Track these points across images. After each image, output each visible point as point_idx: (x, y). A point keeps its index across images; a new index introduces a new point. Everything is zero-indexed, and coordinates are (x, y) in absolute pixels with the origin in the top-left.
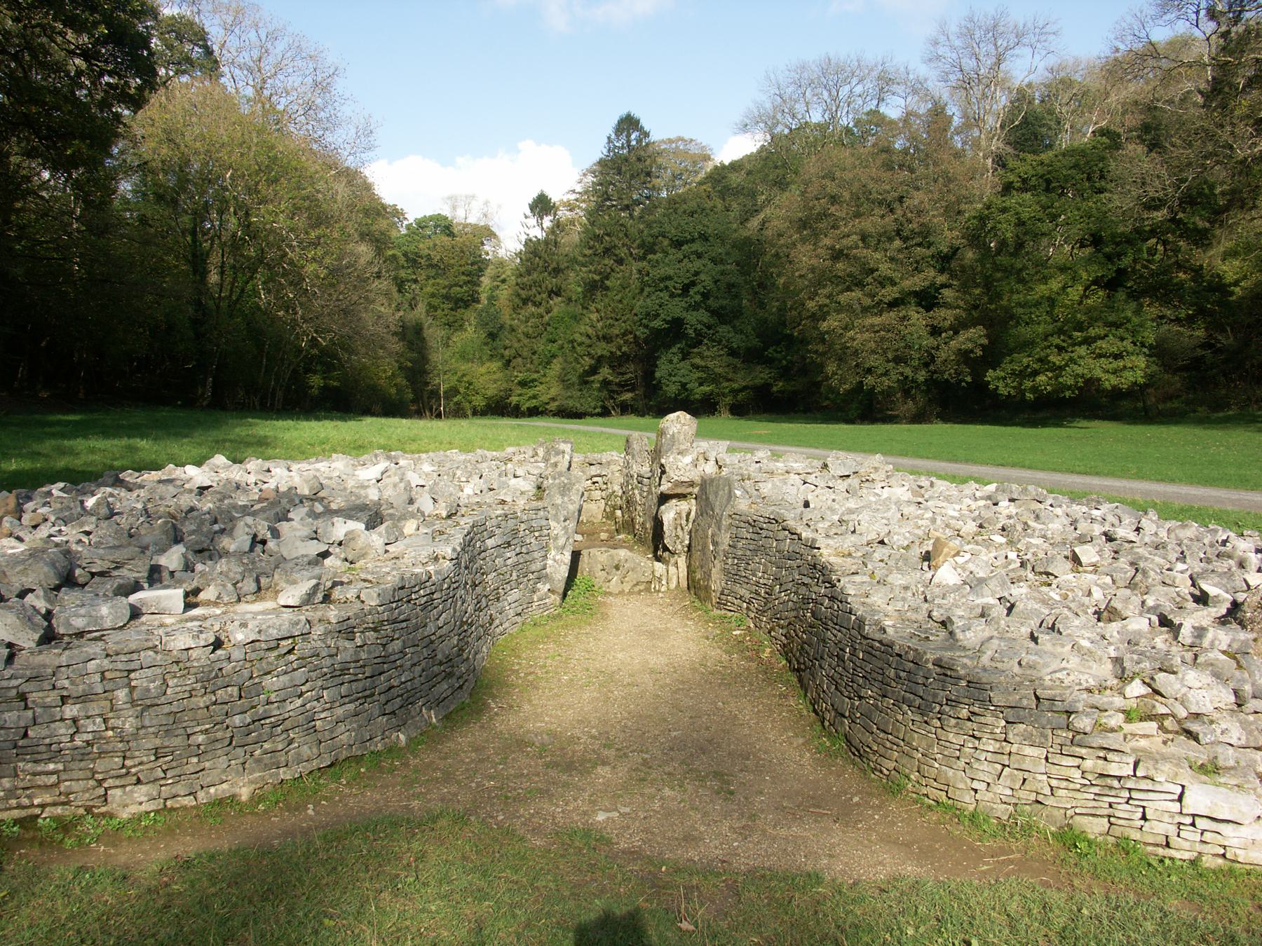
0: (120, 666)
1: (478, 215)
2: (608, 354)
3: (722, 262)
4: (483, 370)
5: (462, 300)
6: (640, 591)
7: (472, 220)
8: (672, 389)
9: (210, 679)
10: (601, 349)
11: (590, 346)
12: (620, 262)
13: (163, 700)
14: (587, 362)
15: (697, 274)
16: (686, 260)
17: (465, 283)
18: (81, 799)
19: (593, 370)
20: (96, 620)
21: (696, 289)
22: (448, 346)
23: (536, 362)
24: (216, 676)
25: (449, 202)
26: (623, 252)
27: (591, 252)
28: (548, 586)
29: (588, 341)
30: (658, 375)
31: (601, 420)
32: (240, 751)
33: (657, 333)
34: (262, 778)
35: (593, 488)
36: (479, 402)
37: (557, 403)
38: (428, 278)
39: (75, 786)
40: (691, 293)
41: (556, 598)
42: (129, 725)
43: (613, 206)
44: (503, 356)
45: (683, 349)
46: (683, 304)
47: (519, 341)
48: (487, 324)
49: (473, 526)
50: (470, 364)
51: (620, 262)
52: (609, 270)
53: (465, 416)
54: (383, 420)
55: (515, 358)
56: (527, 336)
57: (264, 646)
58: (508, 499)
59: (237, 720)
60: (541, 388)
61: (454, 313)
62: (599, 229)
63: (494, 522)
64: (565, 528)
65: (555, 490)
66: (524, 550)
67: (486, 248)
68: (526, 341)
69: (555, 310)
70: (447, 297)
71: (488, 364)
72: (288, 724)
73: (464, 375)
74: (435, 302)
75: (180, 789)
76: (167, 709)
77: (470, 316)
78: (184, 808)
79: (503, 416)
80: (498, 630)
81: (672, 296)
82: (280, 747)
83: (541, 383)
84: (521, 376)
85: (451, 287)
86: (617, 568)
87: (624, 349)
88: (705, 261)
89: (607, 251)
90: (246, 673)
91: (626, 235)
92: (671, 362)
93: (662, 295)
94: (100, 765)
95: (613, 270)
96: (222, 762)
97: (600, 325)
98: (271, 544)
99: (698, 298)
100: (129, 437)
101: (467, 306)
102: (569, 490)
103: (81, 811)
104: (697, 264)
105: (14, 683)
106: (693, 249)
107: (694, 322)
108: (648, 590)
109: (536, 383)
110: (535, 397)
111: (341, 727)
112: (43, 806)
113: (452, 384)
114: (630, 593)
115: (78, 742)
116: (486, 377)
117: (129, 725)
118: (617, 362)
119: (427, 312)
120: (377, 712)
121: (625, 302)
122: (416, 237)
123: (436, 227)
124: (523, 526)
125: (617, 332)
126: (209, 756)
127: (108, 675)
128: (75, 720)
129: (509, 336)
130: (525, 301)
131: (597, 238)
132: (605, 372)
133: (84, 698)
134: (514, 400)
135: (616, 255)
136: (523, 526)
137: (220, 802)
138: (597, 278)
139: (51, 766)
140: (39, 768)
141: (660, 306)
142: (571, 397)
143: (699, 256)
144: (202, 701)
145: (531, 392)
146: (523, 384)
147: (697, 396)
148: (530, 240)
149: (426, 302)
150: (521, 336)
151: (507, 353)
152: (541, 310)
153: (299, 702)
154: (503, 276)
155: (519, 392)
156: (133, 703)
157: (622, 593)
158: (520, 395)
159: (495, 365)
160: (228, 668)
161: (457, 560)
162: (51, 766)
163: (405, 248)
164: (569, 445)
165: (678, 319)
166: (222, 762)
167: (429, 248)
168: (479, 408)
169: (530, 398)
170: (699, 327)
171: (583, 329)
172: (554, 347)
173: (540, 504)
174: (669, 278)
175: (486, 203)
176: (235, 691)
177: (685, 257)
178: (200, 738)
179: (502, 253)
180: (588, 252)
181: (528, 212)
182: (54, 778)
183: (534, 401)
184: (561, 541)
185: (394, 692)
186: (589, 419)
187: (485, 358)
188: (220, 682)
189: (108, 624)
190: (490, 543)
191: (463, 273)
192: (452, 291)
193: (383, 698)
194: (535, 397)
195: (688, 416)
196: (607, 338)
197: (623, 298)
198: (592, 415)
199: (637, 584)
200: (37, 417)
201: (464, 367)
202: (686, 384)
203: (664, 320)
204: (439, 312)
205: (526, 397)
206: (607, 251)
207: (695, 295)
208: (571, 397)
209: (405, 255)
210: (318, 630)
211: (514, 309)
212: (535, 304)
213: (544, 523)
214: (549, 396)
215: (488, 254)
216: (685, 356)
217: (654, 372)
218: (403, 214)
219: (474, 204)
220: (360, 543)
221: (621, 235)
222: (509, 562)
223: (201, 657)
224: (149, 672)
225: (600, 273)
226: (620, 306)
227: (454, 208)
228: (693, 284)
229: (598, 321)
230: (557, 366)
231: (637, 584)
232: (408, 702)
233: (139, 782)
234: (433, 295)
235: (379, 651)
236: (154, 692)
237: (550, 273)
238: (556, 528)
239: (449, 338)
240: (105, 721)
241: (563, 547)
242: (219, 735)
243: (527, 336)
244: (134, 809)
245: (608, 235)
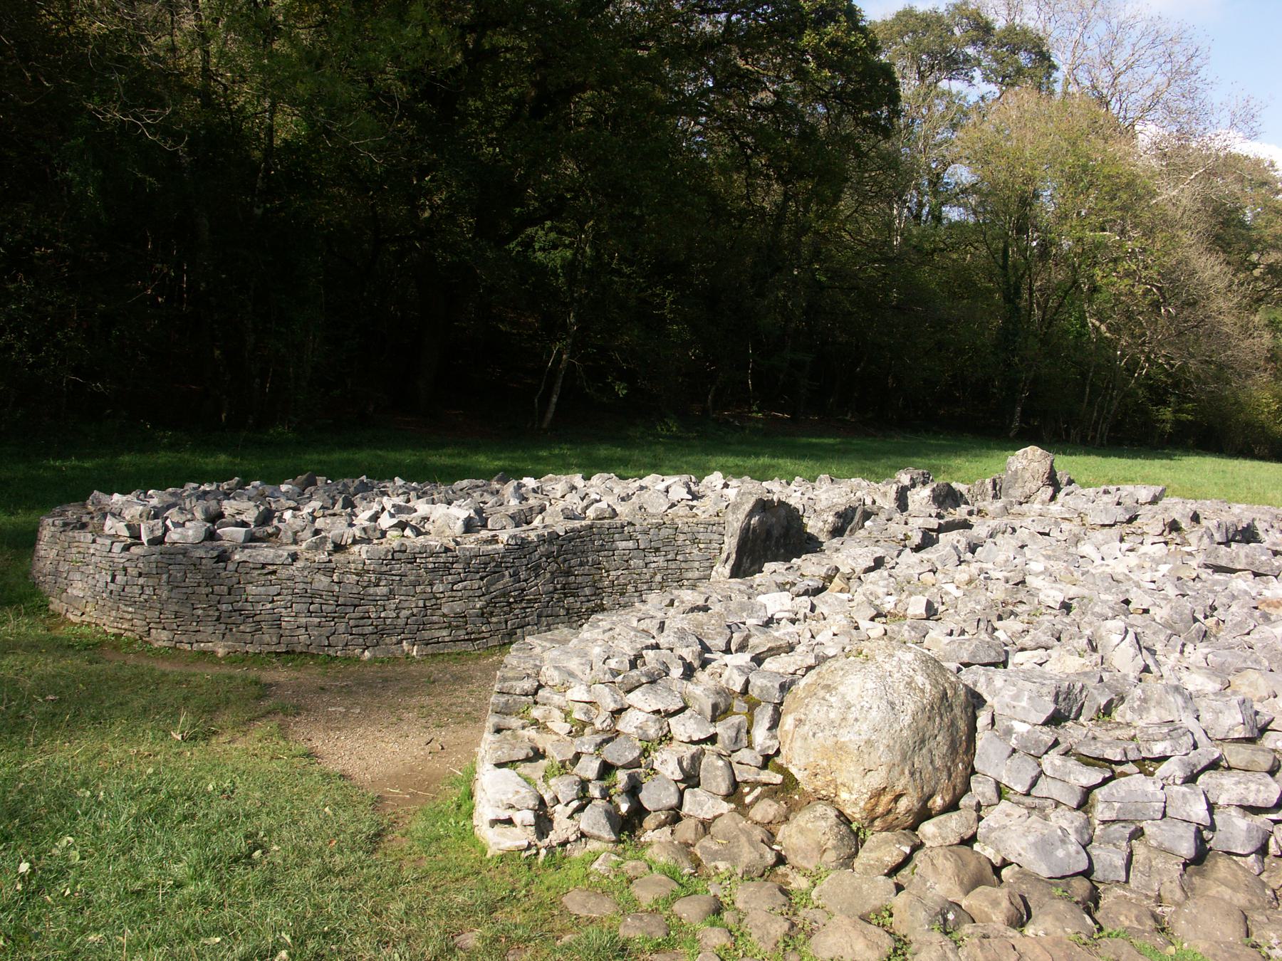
0: (164, 560)
13: (183, 584)
24: (215, 577)
32: (223, 626)
34: (234, 647)
57: (251, 565)
75: (184, 638)
78: (185, 650)
82: (248, 630)
90: (235, 580)
94: (149, 614)
100: (773, 456)
103: (137, 637)
105: (123, 560)
112: (126, 630)
126: (203, 624)
127: (160, 565)
137: (204, 653)
139: (130, 609)
156: (168, 583)
160: (223, 574)
162: (130, 609)
166: (210, 629)
176: (226, 589)
178: (200, 612)
200: (804, 440)
224: (178, 567)
240: (154, 590)
242: (211, 613)
244: (160, 643)
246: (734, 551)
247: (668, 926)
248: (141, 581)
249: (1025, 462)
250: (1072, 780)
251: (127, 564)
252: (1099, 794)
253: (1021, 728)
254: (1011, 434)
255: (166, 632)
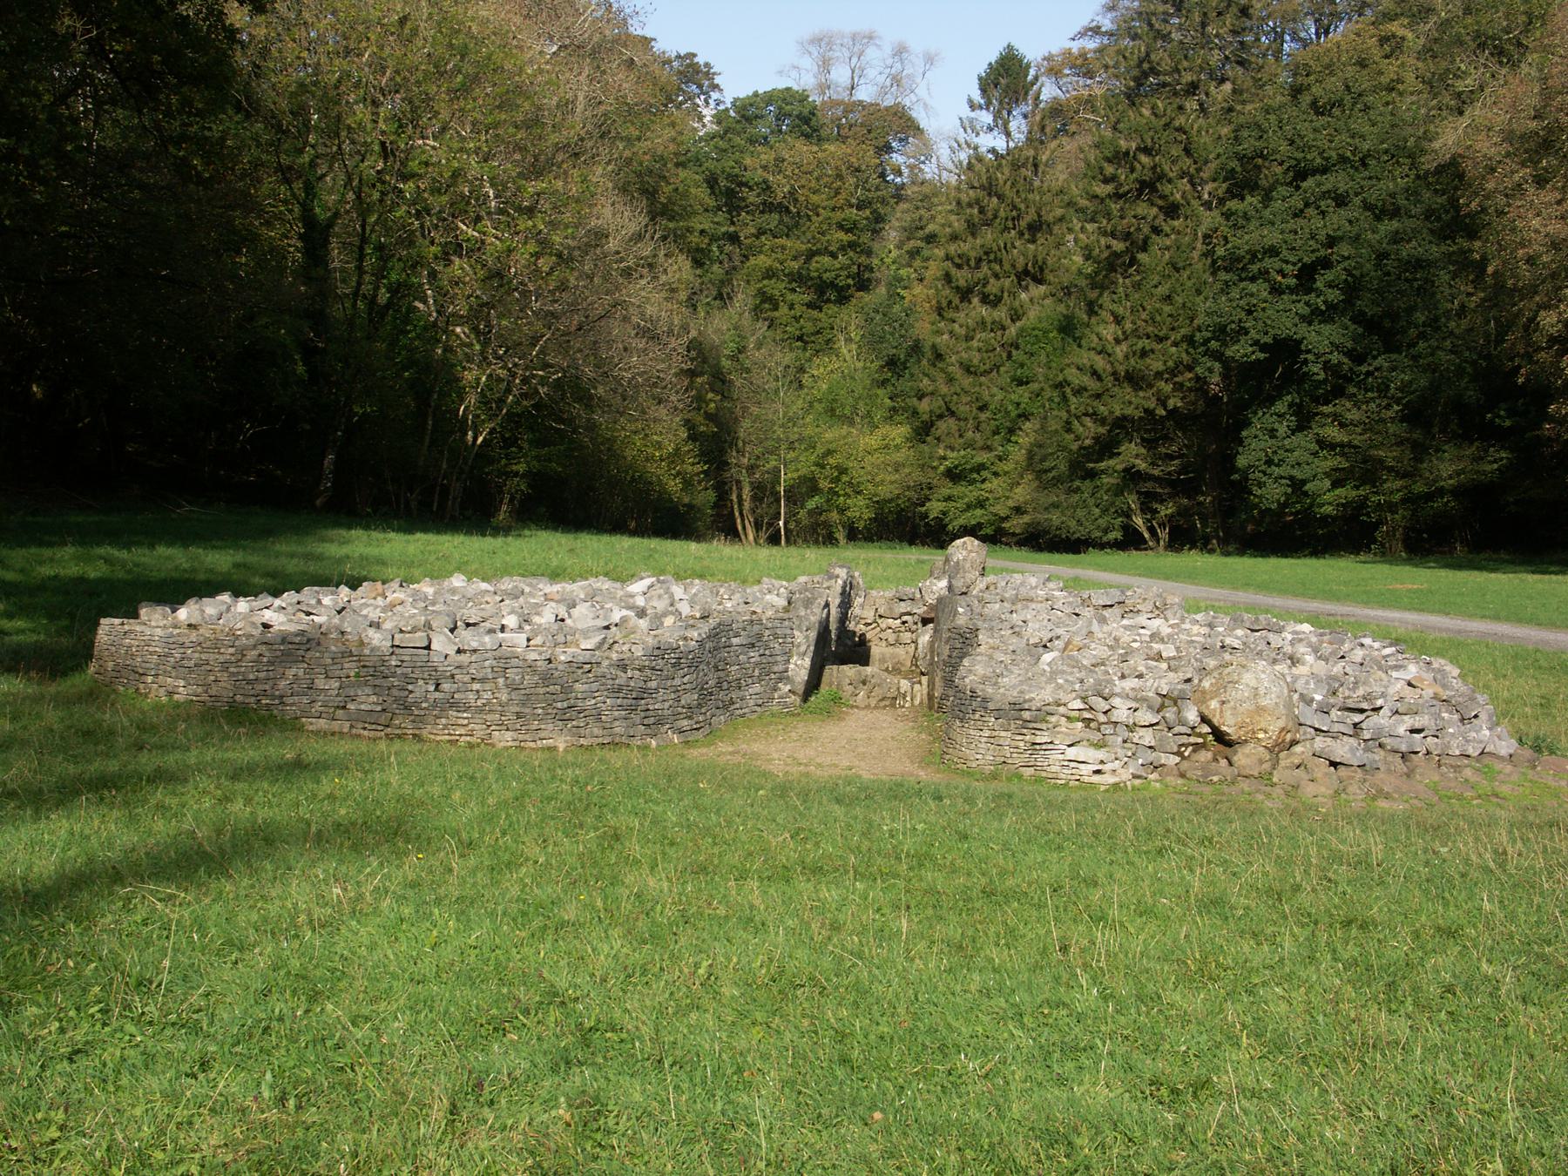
1: (881, 79)
2: (1138, 414)
3: (1395, 213)
4: (873, 441)
5: (833, 285)
6: (886, 706)
7: (864, 94)
8: (1271, 493)
9: (547, 678)
10: (1126, 403)
11: (1098, 396)
12: (1172, 210)
14: (1089, 430)
15: (1332, 242)
16: (1311, 211)
17: (843, 248)
18: (479, 734)
19: (1106, 447)
20: (483, 644)
21: (1329, 275)
22: (801, 386)
23: (987, 428)
25: (813, 50)
26: (1177, 191)
27: (1109, 188)
28: (788, 687)
29: (1093, 385)
30: (1241, 461)
31: (1120, 557)
33: (1239, 374)
35: (903, 629)
36: (860, 510)
37: (1026, 519)
38: (761, 232)
39: (476, 727)
40: (1319, 284)
41: (797, 700)
42: (504, 698)
43: (1164, 85)
44: (915, 413)
45: (1300, 406)
46: (1303, 309)
47: (950, 380)
48: (882, 340)
49: (720, 624)
50: (845, 430)
51: (1172, 210)
52: (1146, 230)
53: (830, 540)
54: (654, 543)
55: (941, 417)
56: (968, 369)
58: (759, 611)
59: (559, 705)
60: (994, 484)
61: (815, 313)
62: (1128, 138)
63: (741, 625)
64: (807, 637)
65: (800, 603)
66: (767, 652)
67: (897, 158)
68: (967, 381)
69: (1033, 314)
70: (798, 278)
71: (885, 429)
72: (587, 713)
73: (829, 453)
74: (776, 287)
76: (523, 692)
77: (849, 321)
79: (911, 543)
80: (738, 712)
81: (1276, 290)
83: (996, 474)
84: (954, 458)
85: (811, 255)
86: (864, 683)
87: (1171, 403)
88: (1354, 211)
89: (1148, 187)
91: (1187, 151)
92: (1272, 433)
93: (1253, 288)
94: (489, 717)
95: (1156, 230)
96: (551, 726)
97: (1120, 351)
98: (568, 621)
99: (1334, 295)
101: (843, 299)
102: (812, 603)
104: (1338, 220)
106: (1328, 186)
107: (1324, 347)
108: (893, 706)
109: (985, 474)
110: (981, 504)
111: (617, 723)
112: (461, 735)
113: (803, 472)
114: (876, 707)
115: (479, 703)
116: (878, 458)
117: (504, 698)
118: (1152, 429)
119: (757, 311)
120: (638, 722)
121: (1179, 300)
122: (737, 140)
123: (780, 117)
124: (767, 633)
125: (1158, 366)
128: (478, 691)
129: (932, 371)
130: (965, 294)
131: (1119, 157)
132: (1132, 453)
133: (483, 680)
134: (934, 508)
135: (1163, 197)
136: (767, 633)
138: (1119, 246)
140: (460, 715)
141: (1249, 312)
142: (1055, 506)
143: (1341, 201)
144: (542, 691)
145: (969, 493)
146: (954, 475)
147: (1328, 509)
148: (980, 159)
149: (752, 290)
150: (955, 370)
151: (924, 406)
152: (1001, 314)
153: (593, 702)
154: (931, 228)
155: (946, 492)
157: (868, 707)
158: (949, 498)
159: (899, 432)
160: (556, 674)
161: (701, 643)
163: (709, 164)
164: (845, 570)
165: (1289, 339)
167: (765, 168)
168: (860, 526)
169: (969, 507)
170: (1335, 358)
171: (1085, 357)
172: (1022, 394)
173: (786, 616)
174: (1272, 251)
175: (900, 51)
177: (1307, 205)
178: (540, 711)
179: (929, 171)
180: (1103, 190)
181: (977, 96)
182: (466, 722)
183: (979, 512)
184: (803, 648)
185: (651, 713)
186: (1093, 556)
187: (878, 416)
188: (552, 681)
189: (489, 647)
190: (735, 641)
191: (841, 227)
192: (814, 265)
193: (643, 714)
194: (981, 504)
195: (976, 542)
196: (1134, 380)
197: (1173, 290)
198: (1102, 546)
199: (883, 699)
201: (832, 434)
202: (1304, 482)
203: (1256, 343)
204: (784, 309)
205: (960, 504)
206: (1148, 187)
207: (1327, 291)
208: (1055, 506)
209: (712, 182)
210: (605, 663)
211: (940, 311)
212: (985, 299)
213: (789, 632)
214: (1011, 503)
215: (899, 173)
216: (1303, 421)
217: (1232, 458)
218: (709, 75)
219: (872, 53)
220: (631, 623)
221: (1176, 151)
222: (752, 660)
223: (542, 665)
225: (1127, 236)
226: (1167, 309)
227: (825, 65)
228: (1326, 263)
229: (1118, 341)
230: (1027, 435)
231: (883, 699)
232: (659, 723)
233: (508, 730)
234: (769, 274)
235: (641, 684)
236: (517, 682)
237: (1021, 234)
238: (799, 637)
239: (802, 370)
241: (804, 654)
243: (968, 369)
245: (1146, 151)
246: (813, 643)
247: (588, 1047)
248: (476, 686)
249: (964, 553)
250: (1348, 721)
251: (455, 672)
252: (1364, 725)
253: (1318, 697)
254: (318, 502)
255: (510, 733)
